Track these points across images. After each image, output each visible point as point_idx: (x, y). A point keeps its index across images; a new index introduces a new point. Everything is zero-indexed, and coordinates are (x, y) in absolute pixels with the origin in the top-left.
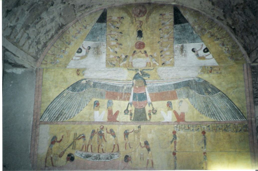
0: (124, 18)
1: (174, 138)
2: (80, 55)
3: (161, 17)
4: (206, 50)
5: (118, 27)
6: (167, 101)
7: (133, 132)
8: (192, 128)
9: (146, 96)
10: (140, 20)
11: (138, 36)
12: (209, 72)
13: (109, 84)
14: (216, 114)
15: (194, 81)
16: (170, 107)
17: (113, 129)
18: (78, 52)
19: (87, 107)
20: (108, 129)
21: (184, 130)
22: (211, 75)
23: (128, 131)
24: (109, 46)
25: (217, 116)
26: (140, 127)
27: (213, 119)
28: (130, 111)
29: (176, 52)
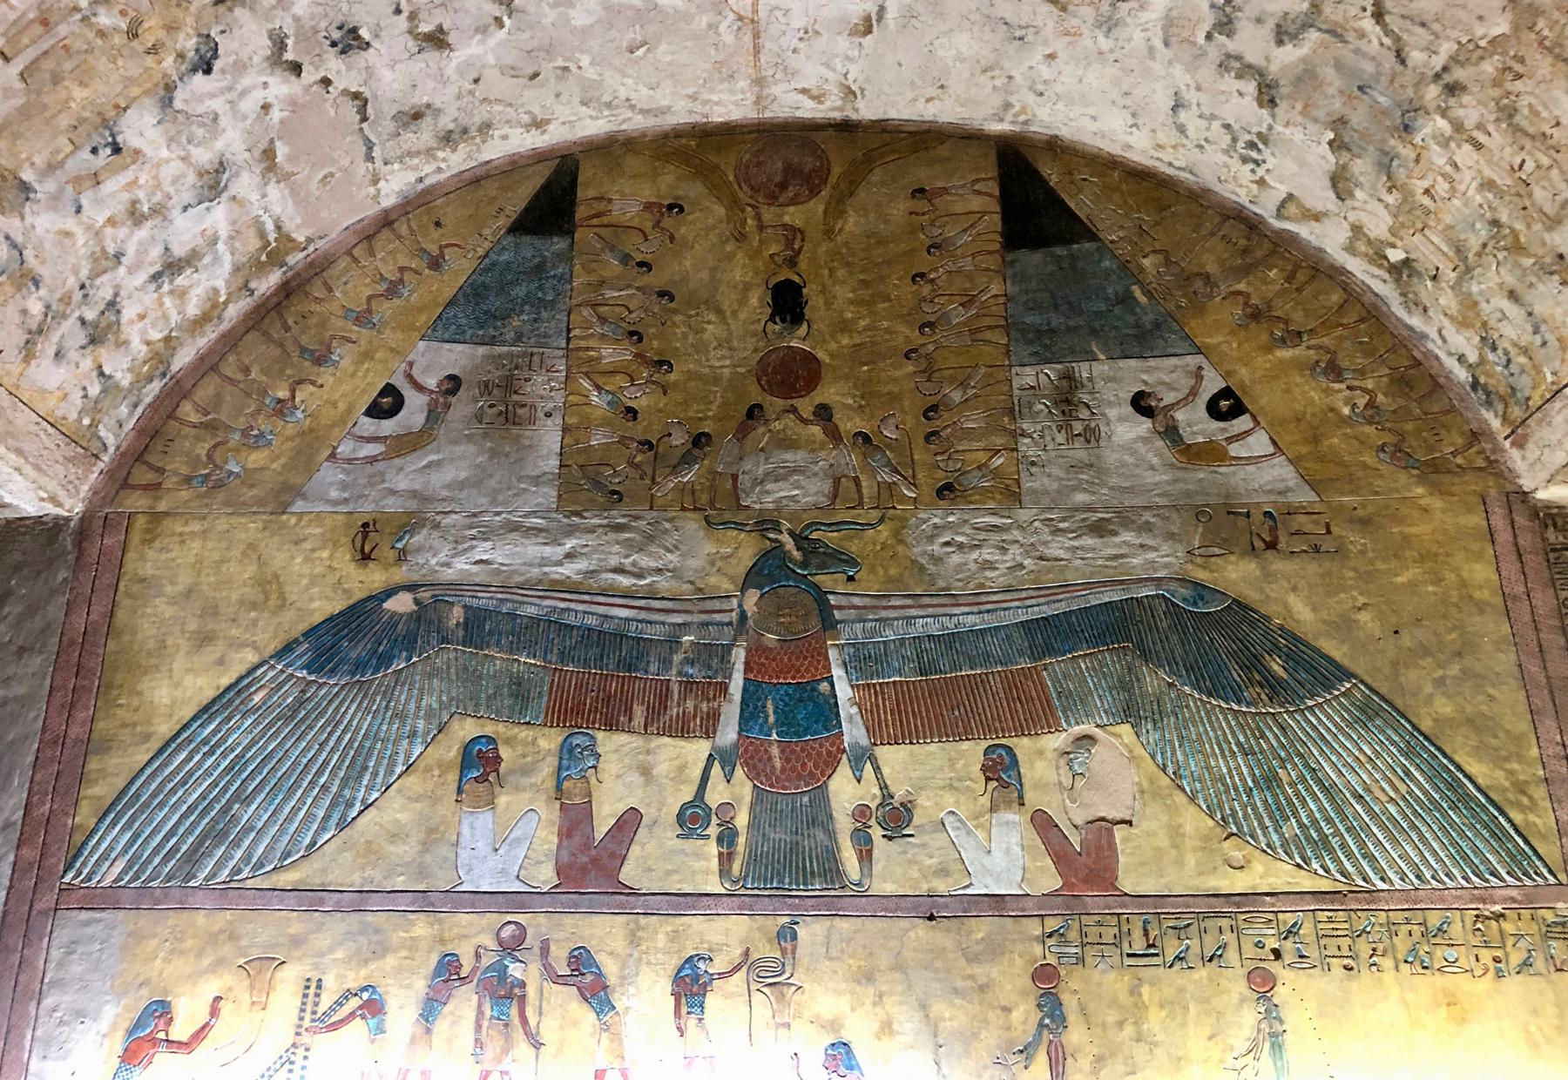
1: (1047, 1021)
2: (388, 426)
3: (922, 205)
4: (1224, 404)
5: (648, 258)
6: (985, 744)
7: (742, 974)
11: (772, 319)
12: (1259, 544)
14: (1335, 842)
15: (1161, 608)
18: (375, 411)
22: (1279, 565)
23: (701, 965)
26: (794, 937)
27: (1321, 871)
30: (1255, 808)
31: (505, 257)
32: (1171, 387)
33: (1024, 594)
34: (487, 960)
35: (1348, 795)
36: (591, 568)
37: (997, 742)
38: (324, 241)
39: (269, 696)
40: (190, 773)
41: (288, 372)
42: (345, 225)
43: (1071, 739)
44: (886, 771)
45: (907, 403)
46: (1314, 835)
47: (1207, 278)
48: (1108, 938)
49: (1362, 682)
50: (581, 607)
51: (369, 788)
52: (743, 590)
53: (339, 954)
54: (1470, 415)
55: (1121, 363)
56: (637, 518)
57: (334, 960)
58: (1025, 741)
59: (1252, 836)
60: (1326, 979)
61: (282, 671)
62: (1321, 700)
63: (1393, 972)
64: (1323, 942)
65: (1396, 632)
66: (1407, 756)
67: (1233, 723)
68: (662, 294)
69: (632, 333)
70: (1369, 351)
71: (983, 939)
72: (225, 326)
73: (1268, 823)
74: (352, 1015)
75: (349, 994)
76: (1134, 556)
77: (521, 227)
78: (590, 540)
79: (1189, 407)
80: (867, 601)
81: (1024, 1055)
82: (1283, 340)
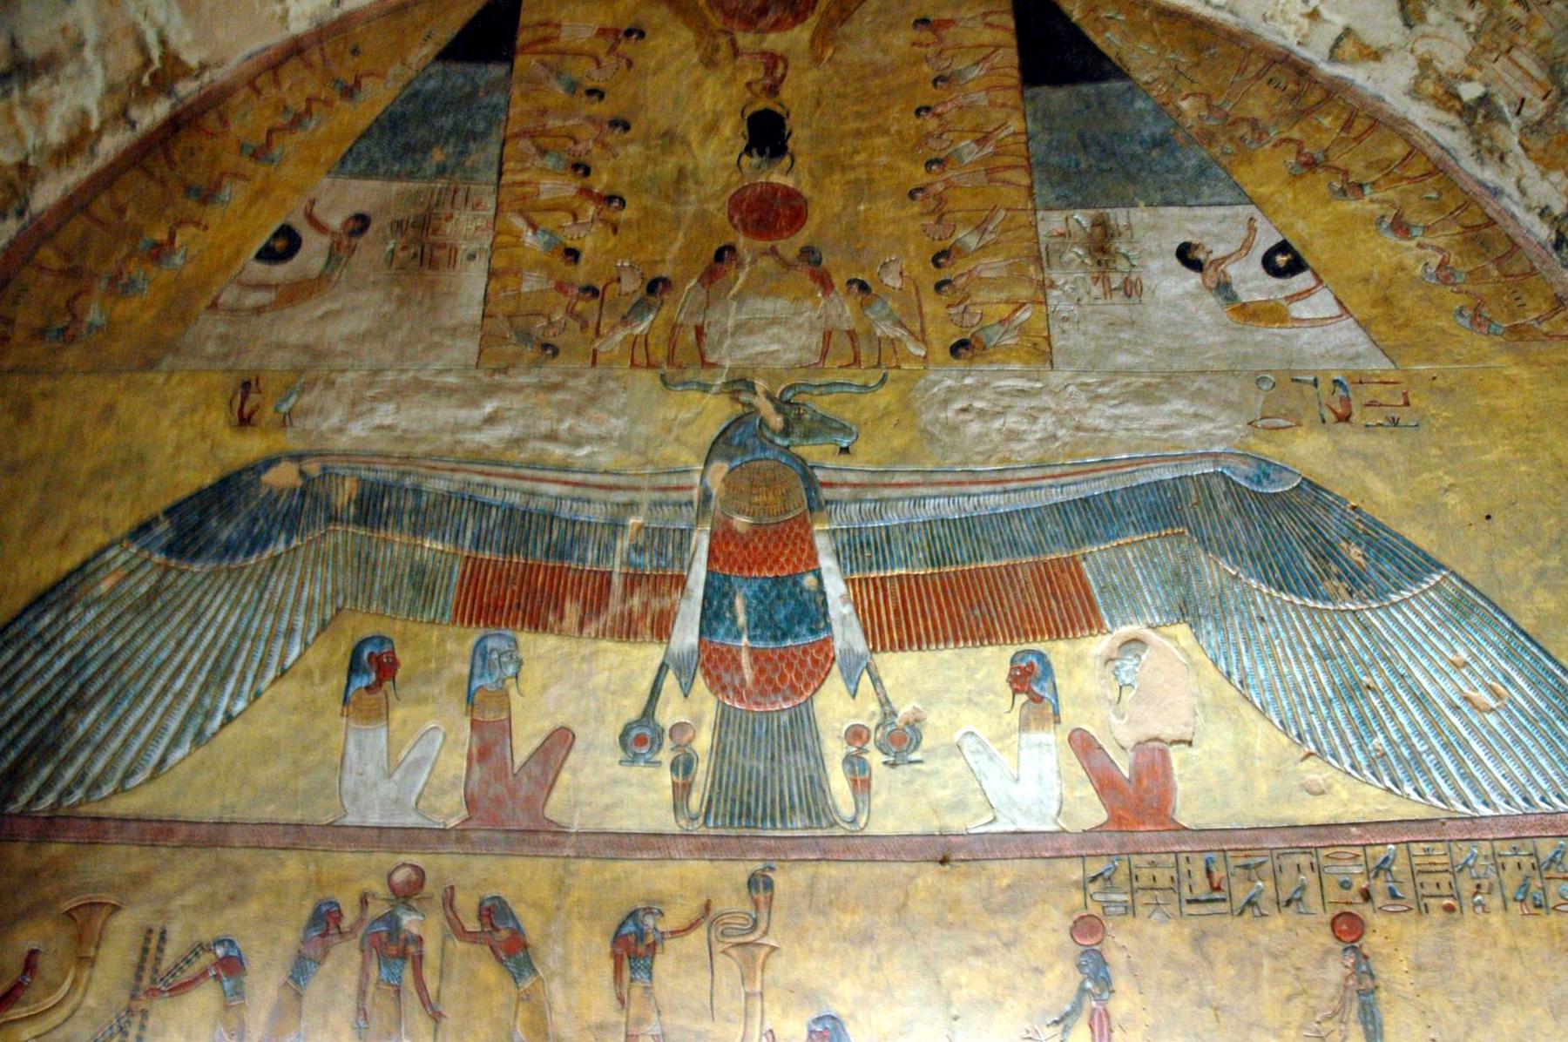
0: (648, 33)
1: (1089, 985)
2: (281, 272)
3: (926, 35)
4: (1281, 260)
5: (602, 85)
6: (1011, 650)
7: (702, 931)
8: (1240, 894)
9: (825, 602)
10: (766, 46)
11: (748, 150)
12: (1329, 416)
13: (499, 498)
14: (1429, 760)
15: (1220, 488)
16: (1037, 699)
17: (507, 894)
18: (268, 255)
19: (289, 687)
20: (460, 899)
21: (1172, 909)
22: (1353, 439)
23: (650, 921)
24: (521, 213)
25: (1447, 776)
26: (769, 885)
27: (1415, 796)
28: (679, 727)
29: (1054, 259)
30: (1336, 723)
31: (432, 85)
32: (1219, 238)
33: (1058, 471)
34: (377, 909)
35: (1443, 706)
36: (516, 435)
37: (1026, 647)
38: (221, 71)
39: (119, 584)
40: (17, 675)
41: (169, 211)
42: (247, 53)
43: (1118, 643)
44: (887, 683)
45: (912, 248)
46: (1406, 753)
47: (1254, 124)
48: (1163, 881)
49: (1453, 573)
50: (501, 482)
51: (235, 696)
52: (707, 463)
53: (190, 898)
54: (1553, 279)
55: (1162, 210)
56: (576, 375)
57: (184, 907)
58: (1062, 645)
59: (1333, 756)
60: (1427, 923)
61: (136, 555)
62: (1407, 594)
63: (1501, 912)
64: (1419, 879)
65: (1488, 517)
66: (1507, 660)
67: (1308, 622)
68: (614, 123)
69: (576, 167)
70: (1439, 207)
71: (1009, 887)
72: (99, 163)
73: (1352, 740)
74: (204, 974)
75: (199, 948)
76: (1187, 426)
77: (455, 52)
78: (516, 402)
79: (1243, 261)
80: (866, 478)
81: (1061, 1026)
82: (1343, 192)
